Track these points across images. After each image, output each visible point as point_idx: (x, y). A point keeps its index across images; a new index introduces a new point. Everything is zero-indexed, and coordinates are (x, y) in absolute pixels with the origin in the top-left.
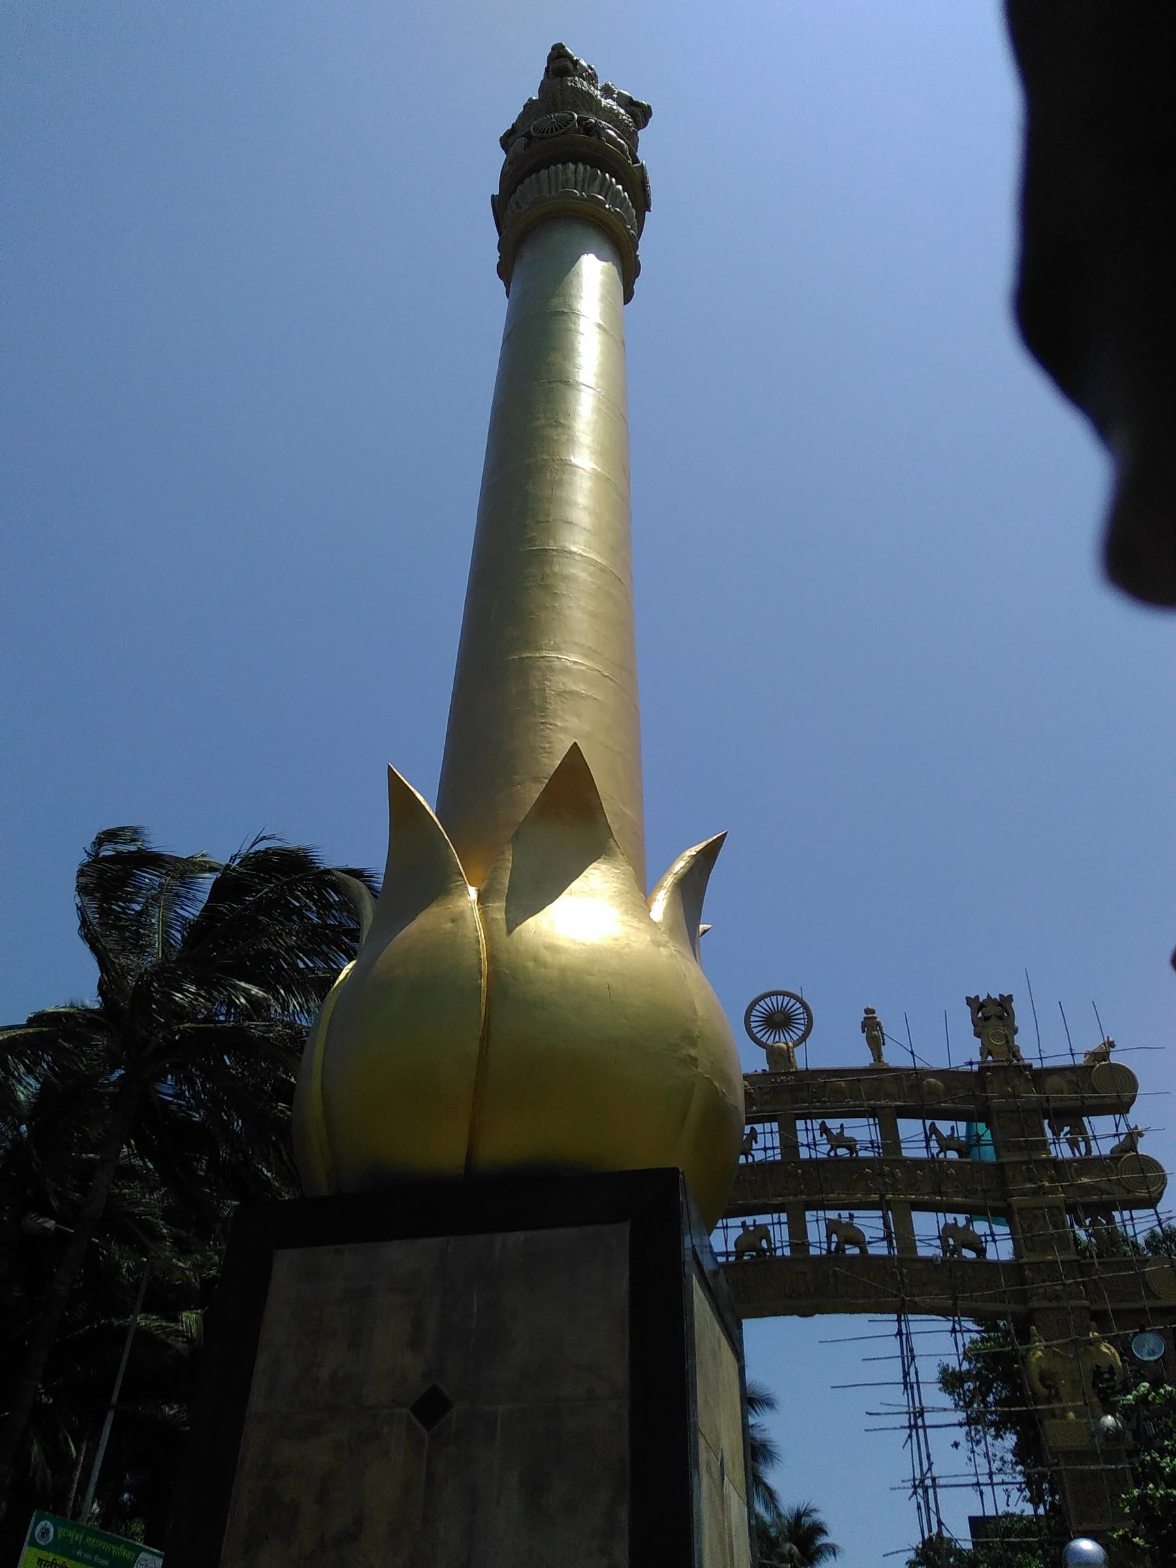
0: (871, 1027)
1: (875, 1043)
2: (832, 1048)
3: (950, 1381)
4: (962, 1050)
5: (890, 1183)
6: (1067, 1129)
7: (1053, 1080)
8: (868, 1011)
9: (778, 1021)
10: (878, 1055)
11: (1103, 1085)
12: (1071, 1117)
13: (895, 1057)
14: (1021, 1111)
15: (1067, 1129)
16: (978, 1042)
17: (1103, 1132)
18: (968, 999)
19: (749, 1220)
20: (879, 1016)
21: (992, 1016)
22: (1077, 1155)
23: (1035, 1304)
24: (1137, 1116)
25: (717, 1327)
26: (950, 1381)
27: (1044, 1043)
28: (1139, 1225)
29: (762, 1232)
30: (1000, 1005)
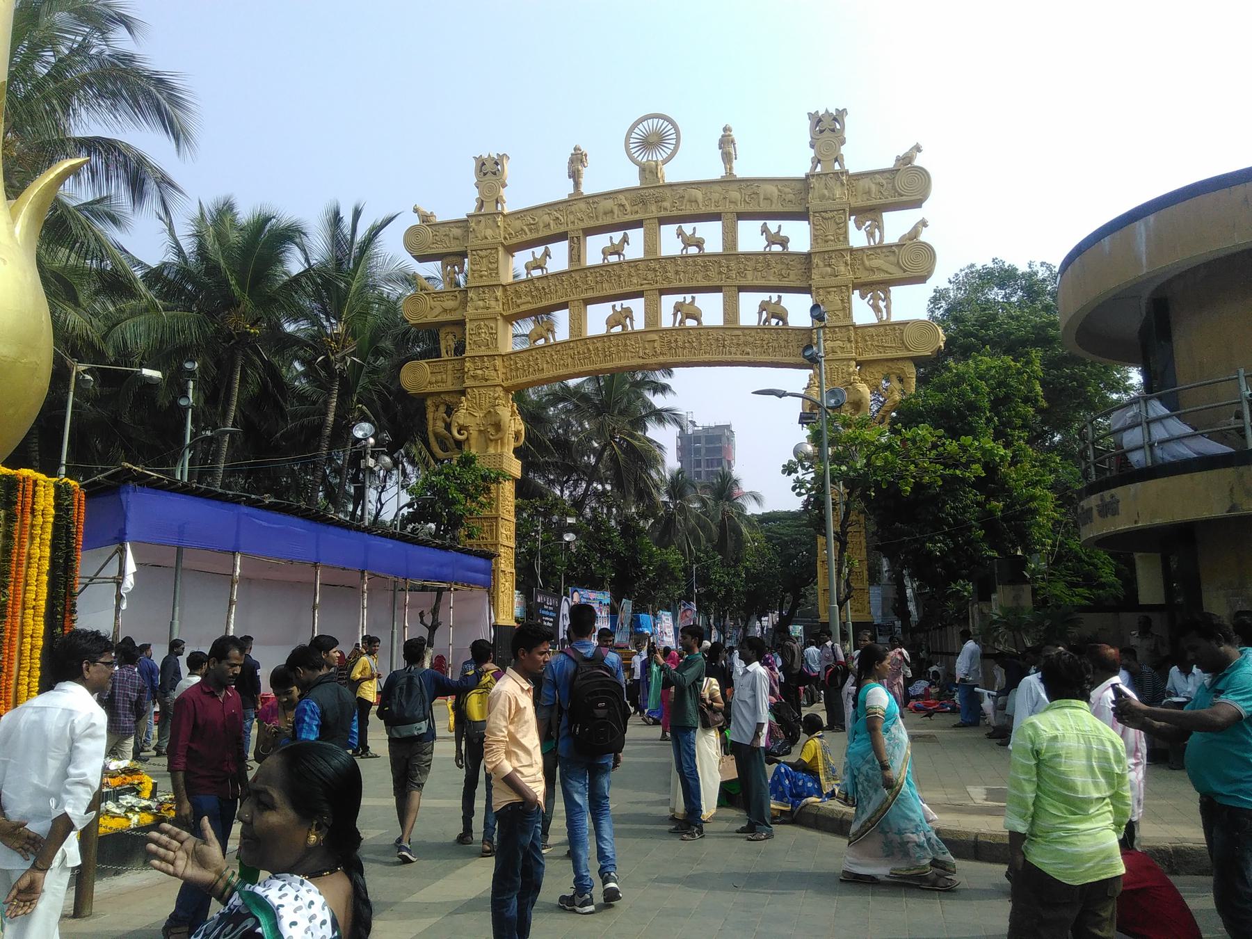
0: (726, 143)
1: (728, 158)
2: (692, 163)
3: (1078, 807)
4: (794, 160)
5: (729, 273)
6: (868, 223)
8: (726, 129)
9: (651, 142)
10: (577, 185)
11: (905, 184)
12: (870, 213)
13: (742, 170)
15: (868, 223)
16: (812, 153)
17: (896, 225)
19: (618, 304)
20: (735, 134)
21: (827, 130)
23: (468, 383)
26: (1078, 807)
27: (864, 154)
29: (628, 313)
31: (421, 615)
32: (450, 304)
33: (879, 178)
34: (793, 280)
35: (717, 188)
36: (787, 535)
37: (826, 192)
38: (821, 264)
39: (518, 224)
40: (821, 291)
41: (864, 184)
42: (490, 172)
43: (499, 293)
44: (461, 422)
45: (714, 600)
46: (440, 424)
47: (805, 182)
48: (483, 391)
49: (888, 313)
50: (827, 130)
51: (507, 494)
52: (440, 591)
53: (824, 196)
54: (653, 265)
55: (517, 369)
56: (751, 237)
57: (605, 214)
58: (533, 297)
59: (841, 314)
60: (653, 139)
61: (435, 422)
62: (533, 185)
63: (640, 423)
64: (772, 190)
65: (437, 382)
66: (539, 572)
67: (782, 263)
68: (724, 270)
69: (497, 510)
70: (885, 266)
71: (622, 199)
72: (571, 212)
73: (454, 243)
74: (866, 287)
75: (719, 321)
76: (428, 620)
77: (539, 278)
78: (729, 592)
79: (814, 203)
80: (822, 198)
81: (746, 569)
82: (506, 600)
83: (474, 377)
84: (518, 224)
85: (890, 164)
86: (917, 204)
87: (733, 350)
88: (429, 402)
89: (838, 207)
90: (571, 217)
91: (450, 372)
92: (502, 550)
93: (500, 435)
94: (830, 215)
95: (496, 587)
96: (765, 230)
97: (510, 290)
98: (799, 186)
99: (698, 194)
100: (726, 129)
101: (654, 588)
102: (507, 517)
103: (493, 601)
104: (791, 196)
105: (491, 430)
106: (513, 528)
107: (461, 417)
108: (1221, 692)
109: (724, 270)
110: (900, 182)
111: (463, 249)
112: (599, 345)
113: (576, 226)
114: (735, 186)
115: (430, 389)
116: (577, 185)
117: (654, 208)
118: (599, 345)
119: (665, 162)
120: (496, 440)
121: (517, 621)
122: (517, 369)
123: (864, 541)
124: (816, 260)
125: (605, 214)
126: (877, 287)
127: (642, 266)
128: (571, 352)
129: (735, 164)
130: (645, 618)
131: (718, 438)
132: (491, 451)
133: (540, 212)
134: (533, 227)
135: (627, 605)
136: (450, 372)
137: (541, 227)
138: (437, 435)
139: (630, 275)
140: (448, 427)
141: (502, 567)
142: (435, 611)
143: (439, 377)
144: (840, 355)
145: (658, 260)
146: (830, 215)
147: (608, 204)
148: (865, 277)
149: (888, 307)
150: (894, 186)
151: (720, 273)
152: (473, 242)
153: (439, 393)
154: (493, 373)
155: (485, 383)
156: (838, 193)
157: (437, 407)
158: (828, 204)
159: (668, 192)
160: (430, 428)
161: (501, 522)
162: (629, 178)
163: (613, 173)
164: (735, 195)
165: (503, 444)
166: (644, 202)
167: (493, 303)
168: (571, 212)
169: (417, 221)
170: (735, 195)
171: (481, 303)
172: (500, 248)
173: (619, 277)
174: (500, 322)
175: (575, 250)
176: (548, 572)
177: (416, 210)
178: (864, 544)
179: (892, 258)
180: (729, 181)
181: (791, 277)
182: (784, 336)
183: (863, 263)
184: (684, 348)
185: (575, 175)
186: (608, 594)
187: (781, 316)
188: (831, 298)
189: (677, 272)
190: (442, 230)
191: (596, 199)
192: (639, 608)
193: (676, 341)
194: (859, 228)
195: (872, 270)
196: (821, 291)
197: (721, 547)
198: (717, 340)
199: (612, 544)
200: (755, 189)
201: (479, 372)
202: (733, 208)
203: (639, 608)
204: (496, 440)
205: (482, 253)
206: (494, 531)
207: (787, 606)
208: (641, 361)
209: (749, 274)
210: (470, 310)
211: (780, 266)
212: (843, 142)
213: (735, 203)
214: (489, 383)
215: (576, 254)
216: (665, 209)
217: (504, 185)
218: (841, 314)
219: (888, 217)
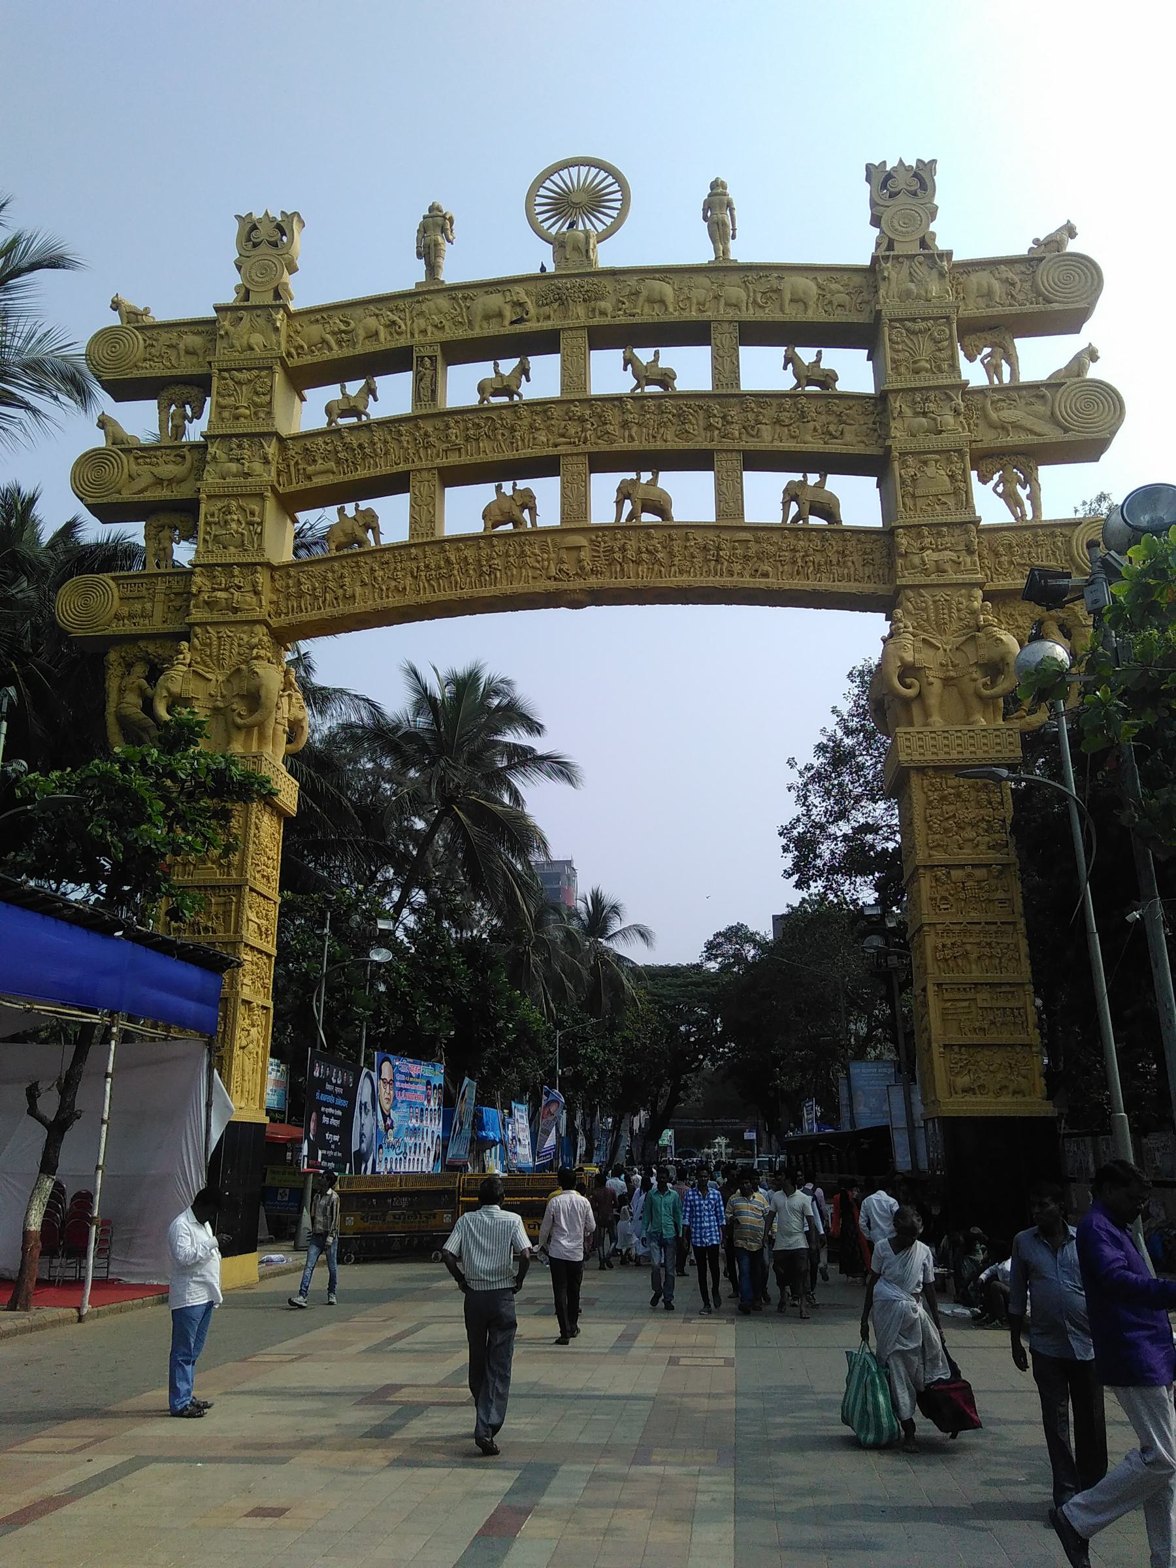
0: (717, 210)
2: (656, 236)
5: (723, 433)
6: (987, 351)
7: (982, 278)
9: (566, 205)
10: (432, 269)
11: (1052, 285)
12: (996, 331)
13: (742, 251)
14: (930, 336)
15: (987, 351)
17: (1039, 358)
18: (869, 168)
20: (732, 193)
21: (902, 192)
22: (996, 381)
23: (197, 615)
24: (1091, 332)
25: (168, 1373)
27: (974, 226)
28: (1067, 492)
29: (528, 501)
30: (916, 175)
31: (32, 1094)
32: (168, 470)
33: (1005, 272)
34: (851, 443)
35: (702, 280)
36: (670, 997)
37: (912, 286)
38: (908, 412)
39: (315, 331)
40: (910, 460)
41: (982, 278)
42: (265, 242)
43: (271, 449)
44: (176, 689)
45: (584, 1092)
46: (133, 702)
47: (872, 273)
48: (225, 631)
49: (1036, 507)
50: (902, 192)
51: (266, 841)
52: (85, 1040)
53: (908, 293)
54: (577, 410)
55: (301, 595)
56: (764, 369)
57: (487, 317)
58: (338, 462)
59: (951, 501)
60: (576, 201)
61: (122, 694)
62: (348, 263)
63: (499, 779)
64: (807, 285)
65: (131, 616)
66: (320, 1017)
67: (829, 412)
68: (717, 422)
69: (242, 869)
70: (1029, 422)
71: (520, 292)
72: (421, 314)
73: (186, 360)
74: (987, 460)
75: (708, 515)
76: (49, 1104)
77: (351, 428)
78: (602, 1074)
79: (889, 303)
80: (906, 295)
81: (626, 1040)
82: (248, 1067)
83: (210, 605)
84: (315, 331)
85: (1021, 248)
86: (1071, 322)
87: (737, 567)
88: (113, 656)
89: (936, 312)
90: (421, 323)
91: (160, 597)
92: (247, 956)
93: (256, 717)
94: (921, 325)
95: (228, 1036)
96: (790, 359)
97: (294, 449)
98: (857, 280)
99: (668, 290)
100: (717, 187)
101: (506, 1062)
102: (260, 887)
103: (220, 1061)
104: (842, 298)
105: (239, 707)
106: (274, 913)
107: (177, 679)
108: (361, 1157)
109: (717, 422)
110: (1046, 276)
111: (204, 370)
112: (469, 553)
113: (429, 338)
114: (735, 278)
115: (116, 629)
116: (432, 269)
117: (581, 310)
118: (469, 553)
119: (602, 237)
120: (249, 729)
121: (269, 1112)
122: (301, 595)
123: (1024, 944)
124: (896, 403)
125: (487, 317)
126: (1017, 461)
127: (556, 412)
128: (414, 565)
129: (732, 244)
130: (491, 1114)
131: (557, 877)
132: (237, 748)
133: (359, 311)
134: (345, 336)
135: (469, 1086)
136: (160, 597)
137: (359, 345)
138: (124, 722)
139: (532, 428)
140: (148, 706)
141: (246, 993)
142: (68, 1085)
143: (137, 607)
144: (953, 577)
145: (591, 401)
146: (921, 325)
147: (495, 301)
148: (989, 439)
149: (1034, 498)
150: (1034, 286)
151: (709, 427)
152: (222, 354)
153: (133, 639)
154: (251, 598)
155: (231, 617)
156: (934, 289)
157: (129, 666)
158: (918, 308)
159: (608, 284)
160: (111, 708)
161: (249, 898)
162: (532, 256)
163: (500, 247)
164: (735, 292)
165: (262, 738)
166: (562, 301)
167: (258, 467)
168: (421, 314)
169: (115, 320)
170: (735, 292)
171: (234, 467)
172: (278, 368)
173: (513, 429)
174: (270, 504)
175: (427, 381)
176: (339, 1020)
177: (116, 305)
178: (1024, 948)
179: (1040, 408)
180: (722, 268)
181: (849, 437)
182: (835, 544)
183: (986, 416)
184: (638, 563)
185: (429, 253)
186: (441, 1068)
187: (828, 509)
188: (930, 471)
189: (625, 425)
190: (165, 337)
191: (470, 293)
192: (484, 1100)
193: (623, 549)
194: (971, 358)
195: (1003, 427)
196: (910, 460)
197: (592, 1005)
198: (705, 549)
199: (453, 977)
200: (775, 283)
201: (221, 595)
202: (731, 314)
203: (484, 1100)
204: (249, 729)
205: (244, 376)
206: (232, 915)
207: (662, 1104)
208: (552, 585)
209: (766, 432)
210: (210, 476)
211: (824, 418)
212: (933, 214)
213: (737, 306)
214: (240, 616)
215: (427, 390)
216: (603, 313)
217: (292, 269)
218: (951, 501)
219: (1024, 346)
